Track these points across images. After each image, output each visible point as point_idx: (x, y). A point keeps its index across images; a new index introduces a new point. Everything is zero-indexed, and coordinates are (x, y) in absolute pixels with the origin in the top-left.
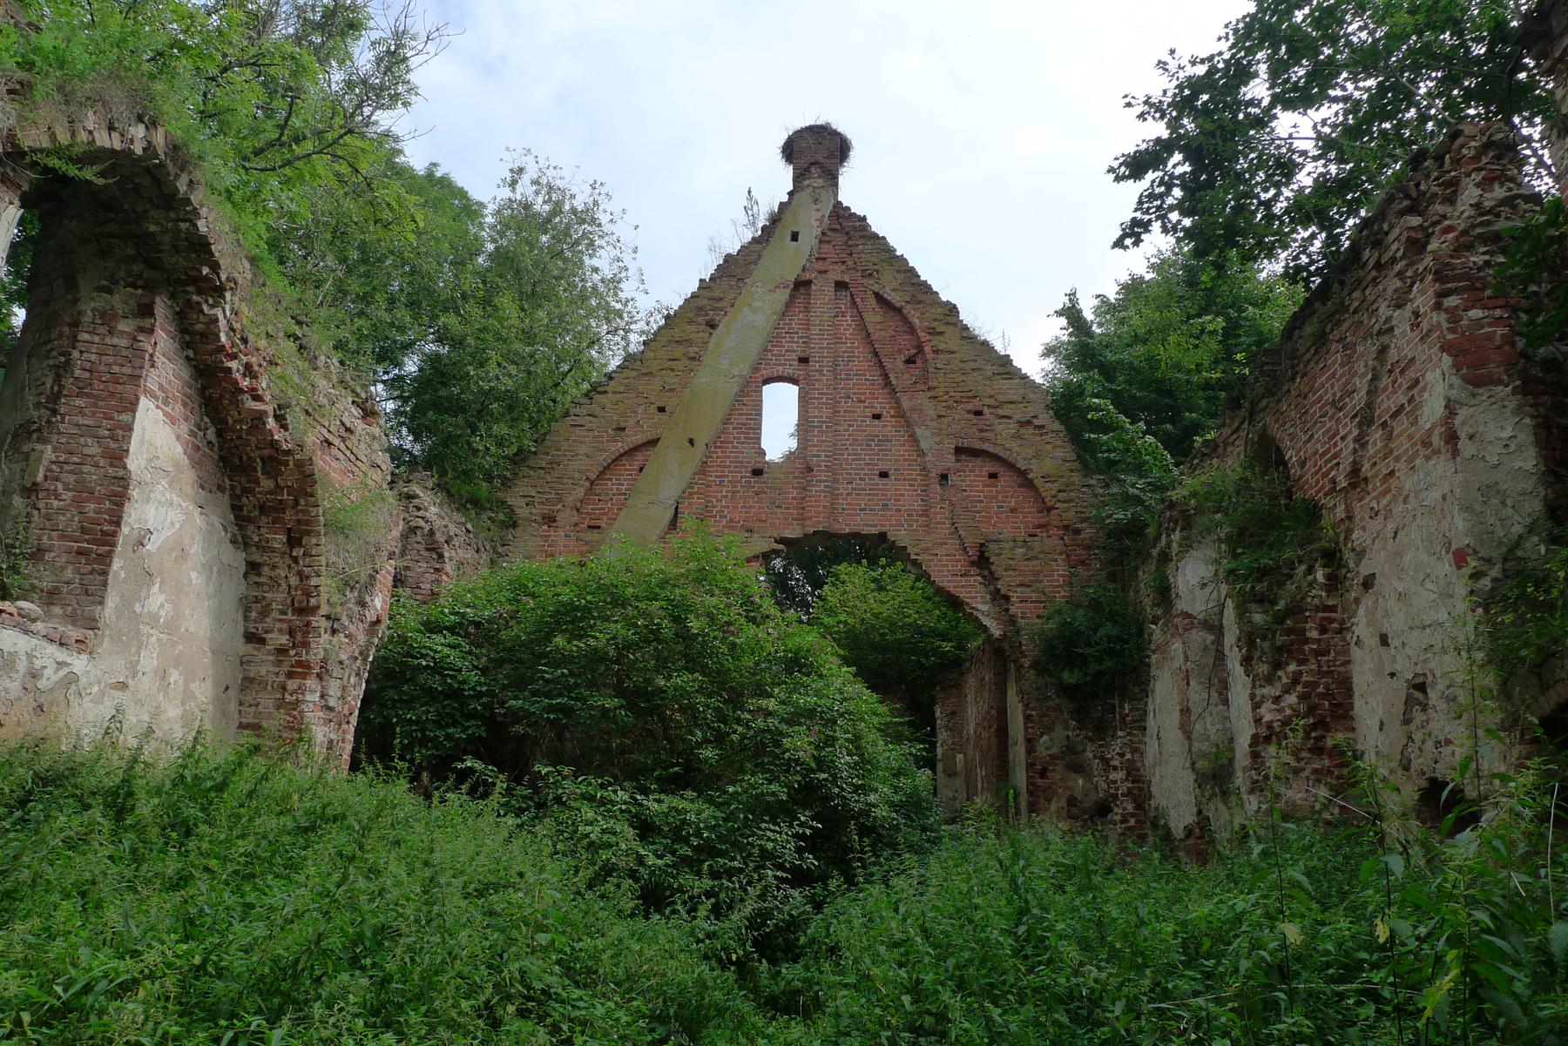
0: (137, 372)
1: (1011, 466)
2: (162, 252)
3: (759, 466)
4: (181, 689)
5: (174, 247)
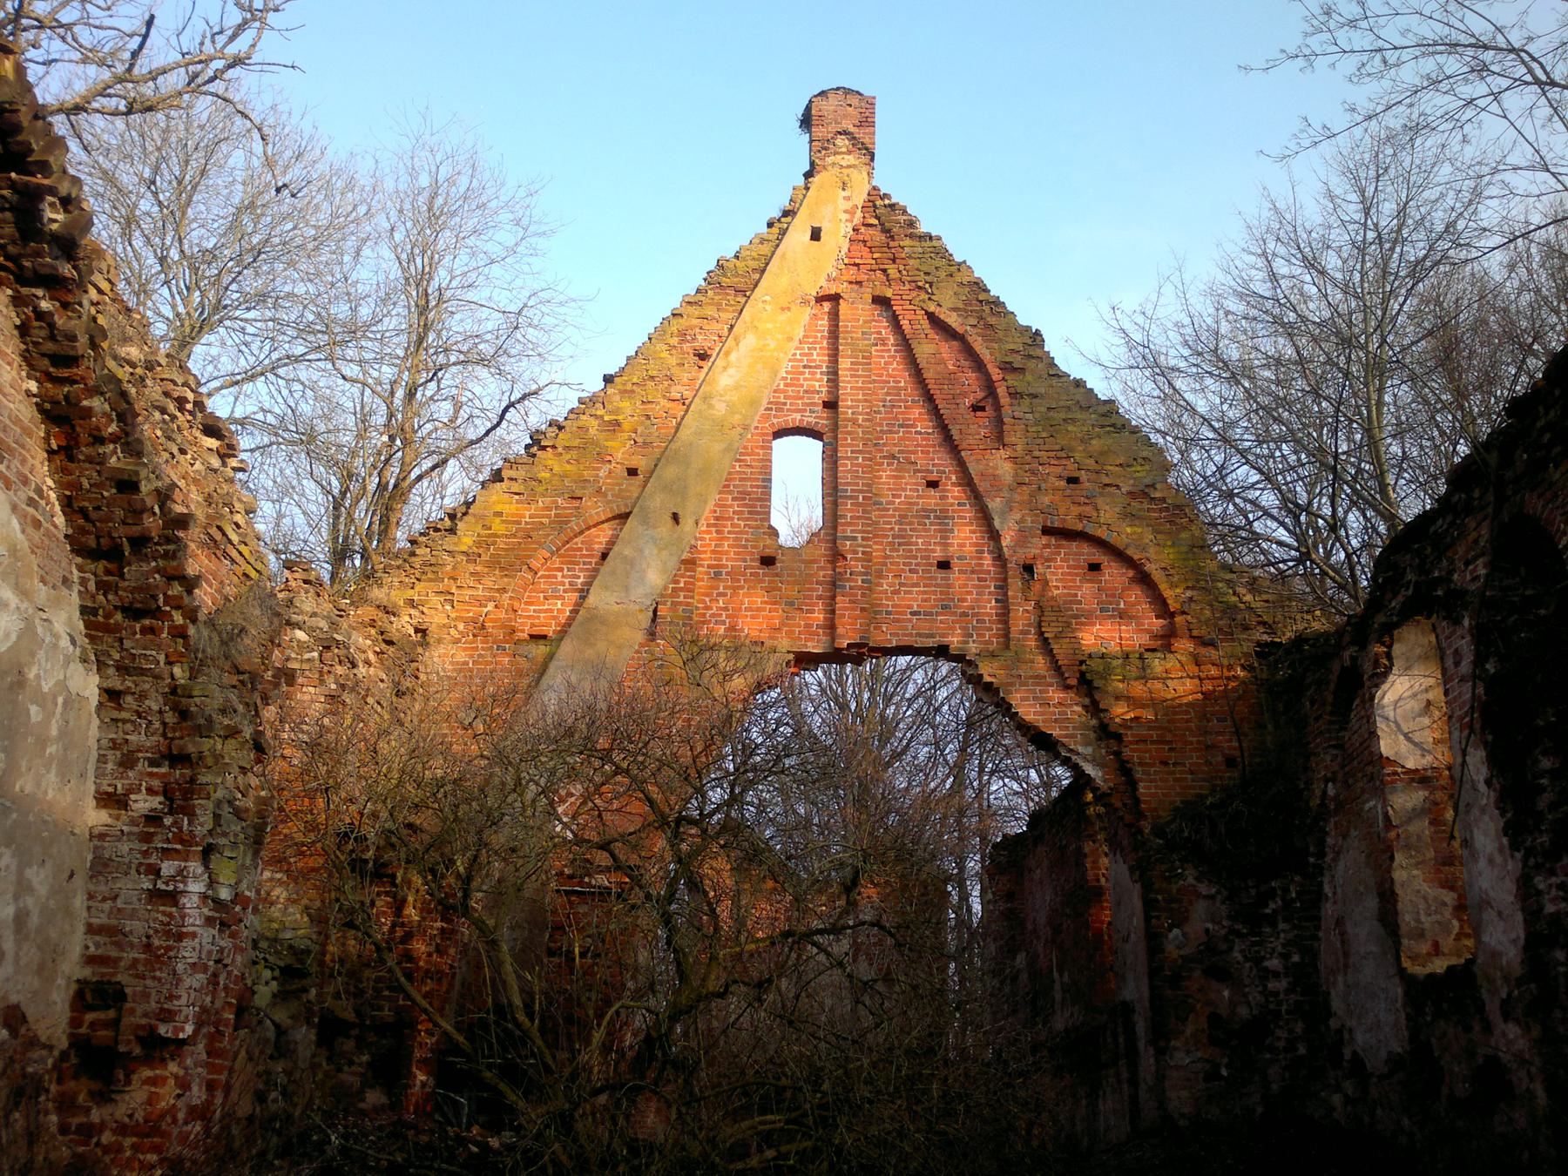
1: (1119, 555)
3: (768, 552)
4: (13, 877)
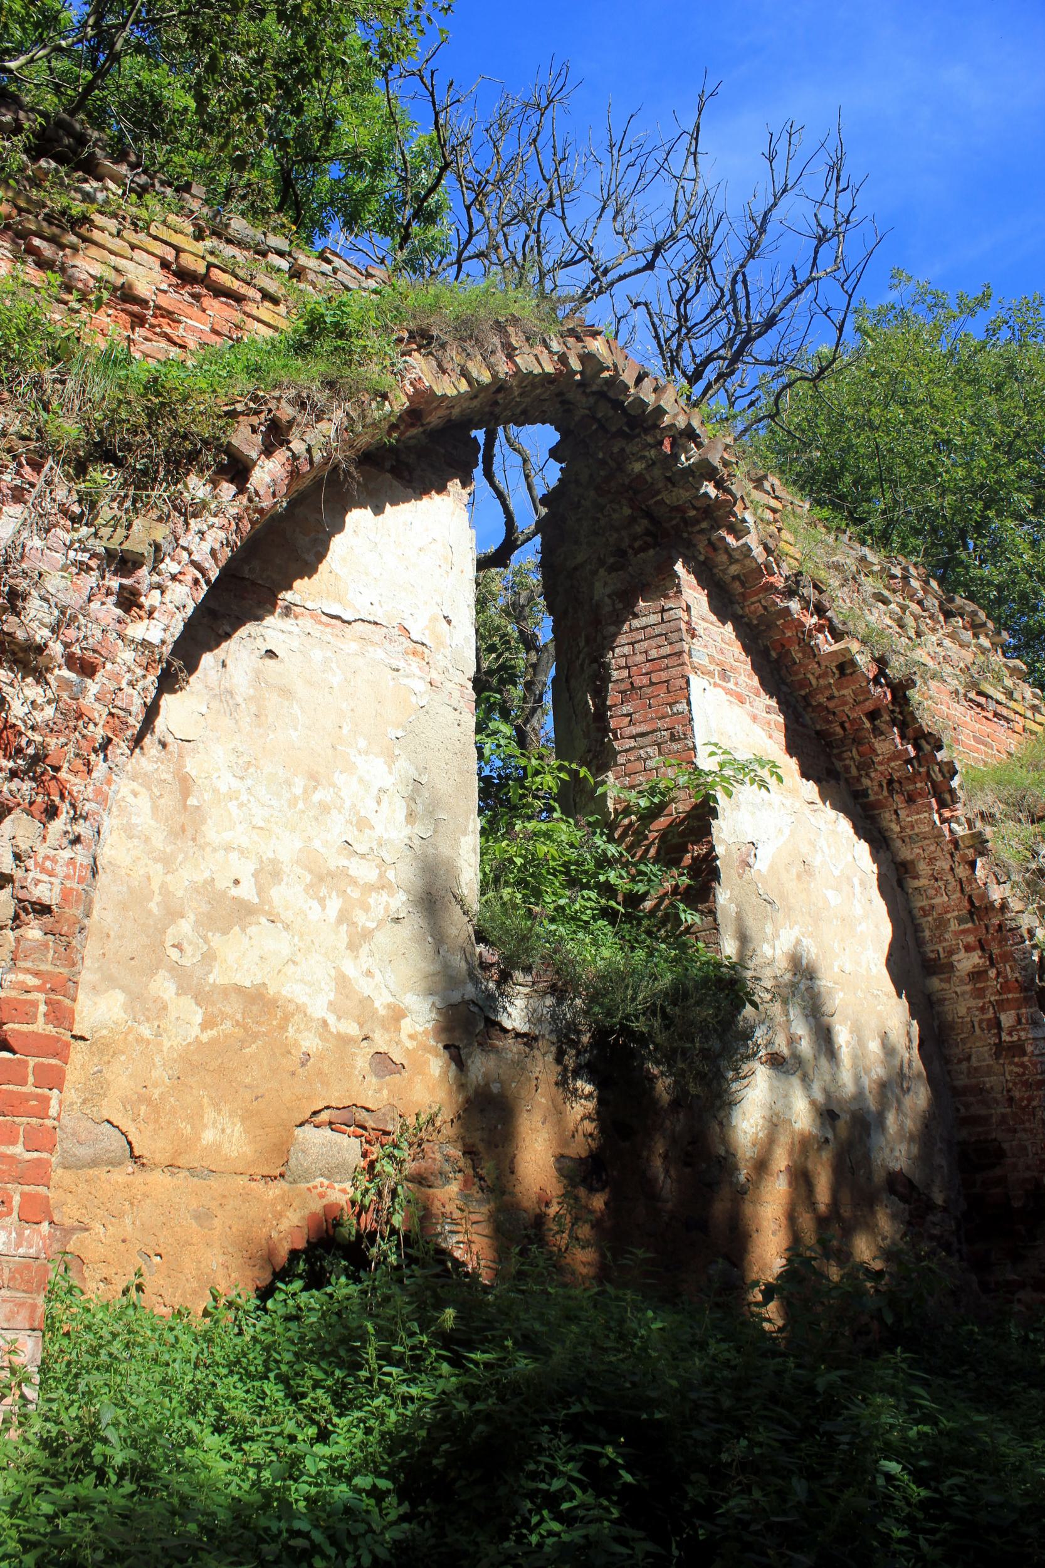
0: (677, 648)
2: (658, 492)
5: (669, 479)
